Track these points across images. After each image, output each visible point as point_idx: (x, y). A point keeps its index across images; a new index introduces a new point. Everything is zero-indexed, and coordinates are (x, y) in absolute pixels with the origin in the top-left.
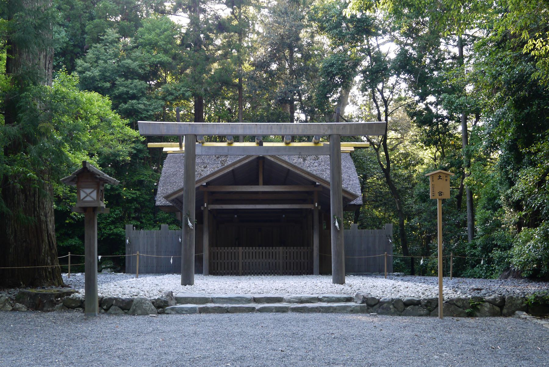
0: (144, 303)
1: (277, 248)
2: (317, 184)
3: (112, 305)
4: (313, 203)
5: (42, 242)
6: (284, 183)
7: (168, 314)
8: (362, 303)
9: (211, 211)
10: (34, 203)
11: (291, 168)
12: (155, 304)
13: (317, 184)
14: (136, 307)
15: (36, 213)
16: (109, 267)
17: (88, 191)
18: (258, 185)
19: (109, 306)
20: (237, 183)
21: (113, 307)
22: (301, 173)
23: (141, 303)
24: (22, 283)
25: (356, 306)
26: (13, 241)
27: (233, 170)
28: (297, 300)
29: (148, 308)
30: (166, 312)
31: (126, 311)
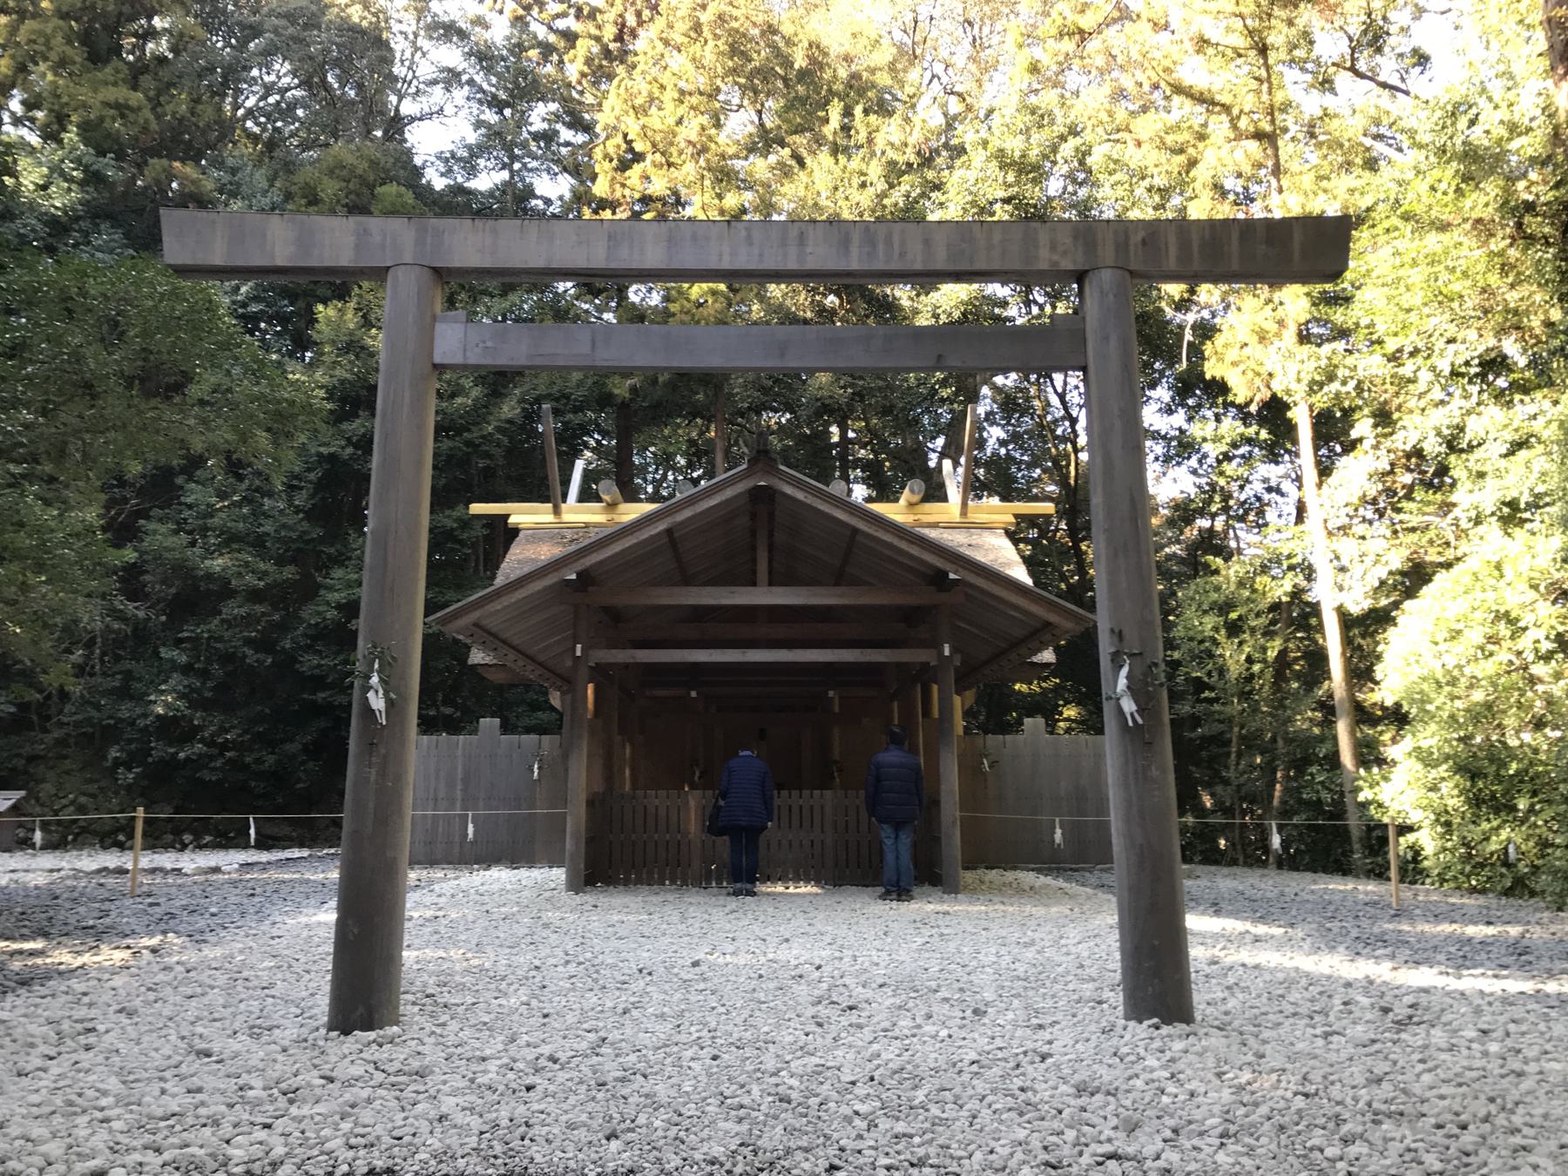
6: (839, 578)
13: (952, 576)
18: (754, 584)
20: (687, 580)
27: (669, 532)
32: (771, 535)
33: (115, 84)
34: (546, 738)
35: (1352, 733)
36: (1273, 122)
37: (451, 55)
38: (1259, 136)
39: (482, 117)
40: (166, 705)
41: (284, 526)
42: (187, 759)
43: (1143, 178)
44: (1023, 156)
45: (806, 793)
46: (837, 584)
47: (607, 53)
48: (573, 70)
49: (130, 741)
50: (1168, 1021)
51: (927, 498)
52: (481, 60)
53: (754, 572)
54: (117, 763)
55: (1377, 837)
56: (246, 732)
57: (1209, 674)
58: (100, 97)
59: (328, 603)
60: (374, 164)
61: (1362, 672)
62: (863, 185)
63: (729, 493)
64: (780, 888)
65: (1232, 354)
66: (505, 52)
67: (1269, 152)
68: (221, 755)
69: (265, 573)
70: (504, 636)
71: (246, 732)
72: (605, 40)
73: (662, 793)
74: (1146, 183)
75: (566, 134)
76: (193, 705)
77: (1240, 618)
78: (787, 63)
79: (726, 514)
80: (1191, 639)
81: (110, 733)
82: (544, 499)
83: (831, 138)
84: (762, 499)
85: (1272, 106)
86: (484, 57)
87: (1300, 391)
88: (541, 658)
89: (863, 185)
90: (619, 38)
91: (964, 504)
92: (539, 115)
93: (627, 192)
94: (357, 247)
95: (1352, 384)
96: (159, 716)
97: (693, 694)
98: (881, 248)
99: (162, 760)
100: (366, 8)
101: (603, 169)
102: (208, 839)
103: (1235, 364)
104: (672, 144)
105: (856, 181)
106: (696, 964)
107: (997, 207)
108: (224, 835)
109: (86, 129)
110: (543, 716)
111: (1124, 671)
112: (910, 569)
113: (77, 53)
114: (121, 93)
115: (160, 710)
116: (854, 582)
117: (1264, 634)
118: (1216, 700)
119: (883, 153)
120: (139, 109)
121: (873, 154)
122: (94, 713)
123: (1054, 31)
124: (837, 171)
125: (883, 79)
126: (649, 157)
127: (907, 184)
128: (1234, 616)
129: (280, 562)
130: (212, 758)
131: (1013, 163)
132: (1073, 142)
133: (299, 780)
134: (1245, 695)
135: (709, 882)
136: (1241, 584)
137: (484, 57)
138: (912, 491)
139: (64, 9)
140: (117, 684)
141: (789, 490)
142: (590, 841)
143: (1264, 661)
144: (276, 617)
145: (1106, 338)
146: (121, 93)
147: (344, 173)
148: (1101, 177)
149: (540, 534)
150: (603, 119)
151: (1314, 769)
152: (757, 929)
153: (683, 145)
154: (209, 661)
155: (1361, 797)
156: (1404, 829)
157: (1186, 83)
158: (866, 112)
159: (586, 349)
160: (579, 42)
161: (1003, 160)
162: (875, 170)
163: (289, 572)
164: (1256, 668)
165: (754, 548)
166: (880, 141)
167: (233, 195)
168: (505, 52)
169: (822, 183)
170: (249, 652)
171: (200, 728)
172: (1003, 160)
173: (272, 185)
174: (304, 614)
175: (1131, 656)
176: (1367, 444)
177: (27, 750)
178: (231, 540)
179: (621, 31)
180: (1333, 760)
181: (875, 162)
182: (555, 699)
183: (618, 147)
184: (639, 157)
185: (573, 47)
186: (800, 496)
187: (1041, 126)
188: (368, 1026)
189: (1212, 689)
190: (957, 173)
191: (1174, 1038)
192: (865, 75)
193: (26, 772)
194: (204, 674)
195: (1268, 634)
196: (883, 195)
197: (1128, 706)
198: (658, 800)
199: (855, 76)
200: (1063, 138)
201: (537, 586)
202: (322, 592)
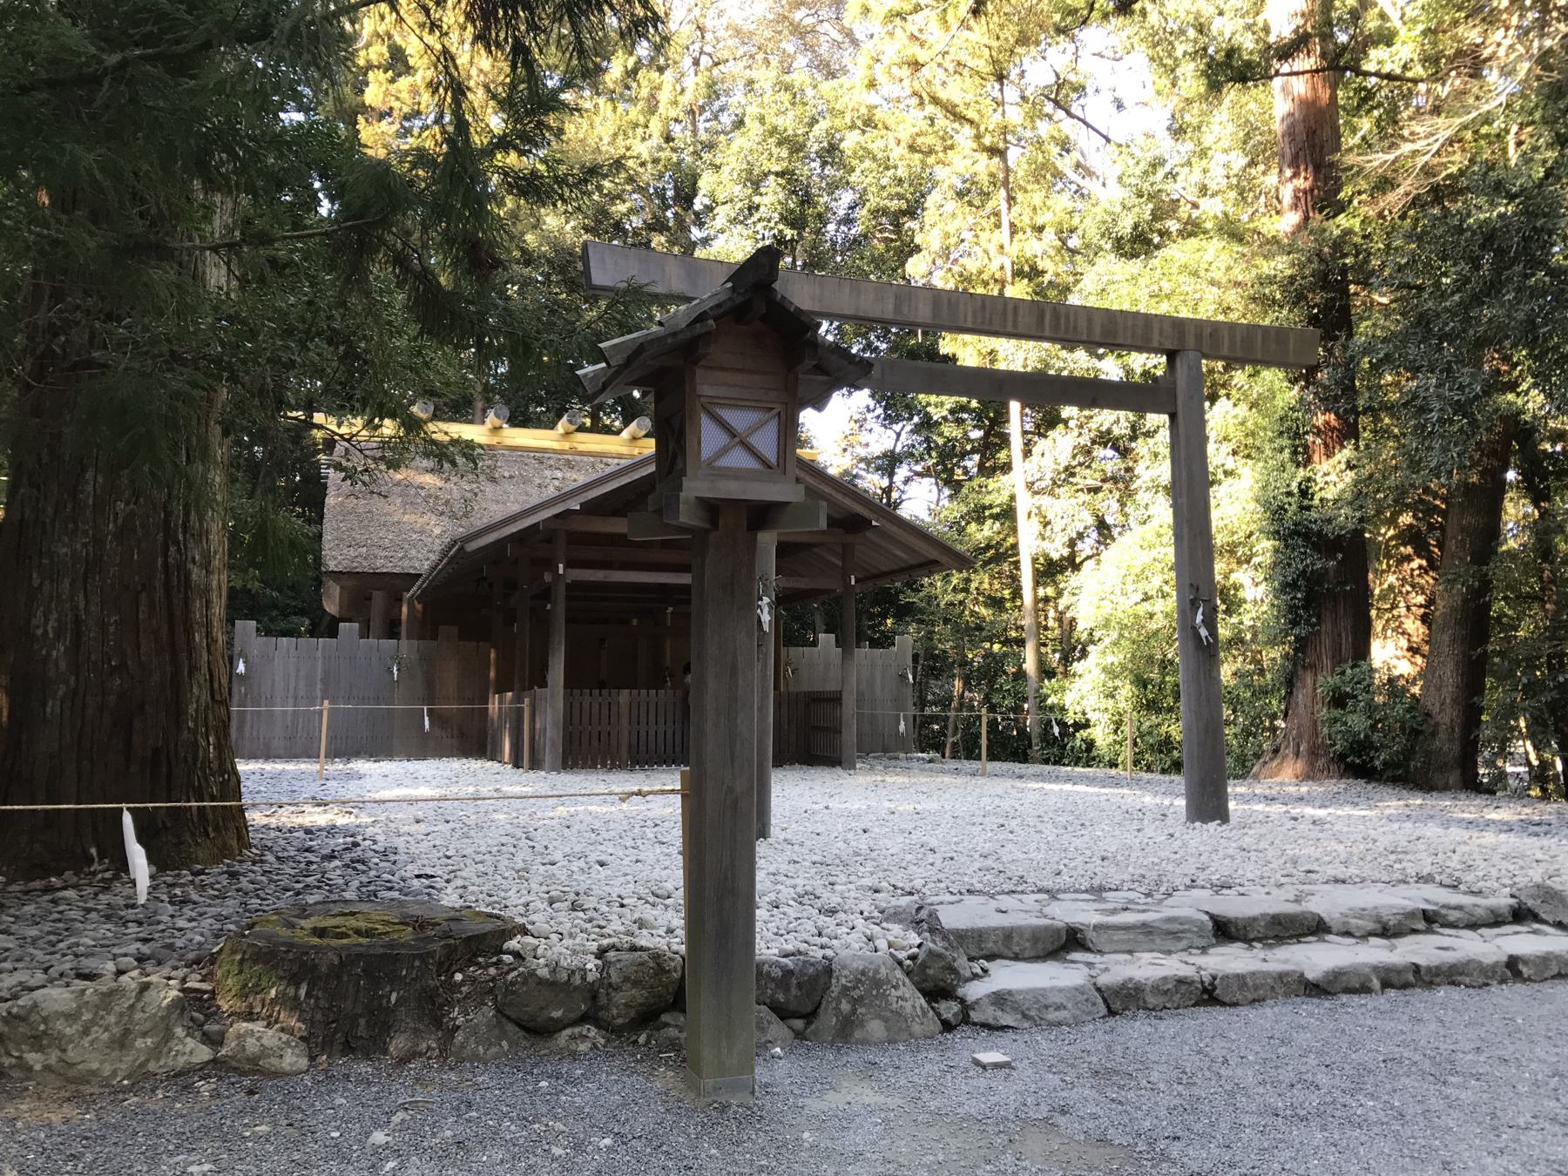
5: (191, 673)
9: (574, 586)
10: (168, 514)
14: (855, 1002)
15: (173, 549)
24: (93, 851)
26: (63, 665)
28: (1371, 926)
31: (799, 1024)
107: (772, 178)
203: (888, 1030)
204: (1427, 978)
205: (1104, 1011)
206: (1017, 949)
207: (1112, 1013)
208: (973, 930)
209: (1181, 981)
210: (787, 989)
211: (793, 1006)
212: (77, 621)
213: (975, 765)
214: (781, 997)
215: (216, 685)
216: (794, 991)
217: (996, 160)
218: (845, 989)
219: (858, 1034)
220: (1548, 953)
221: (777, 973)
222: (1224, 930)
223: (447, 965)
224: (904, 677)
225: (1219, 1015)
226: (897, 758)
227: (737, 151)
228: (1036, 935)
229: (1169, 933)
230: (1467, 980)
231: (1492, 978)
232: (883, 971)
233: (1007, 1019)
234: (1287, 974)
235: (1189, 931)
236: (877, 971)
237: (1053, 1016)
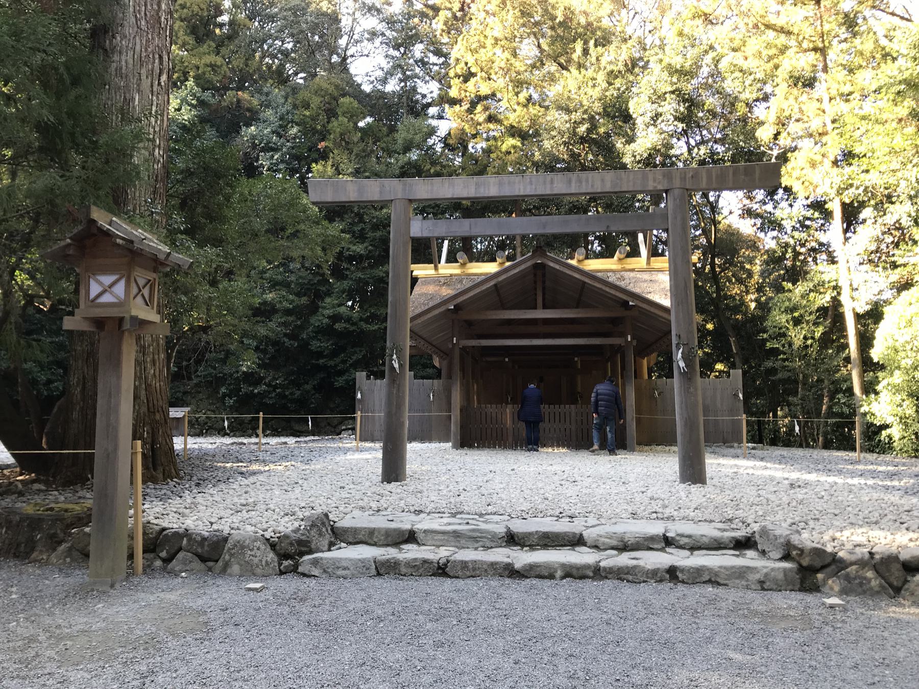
0: (248, 547)
1: (567, 406)
2: (631, 303)
3: (180, 549)
4: (623, 335)
6: (578, 304)
7: (304, 575)
8: (781, 559)
9: (464, 349)
11: (587, 280)
12: (278, 548)
13: (631, 303)
14: (232, 555)
16: (349, 429)
17: (107, 280)
18: (536, 308)
19: (173, 551)
20: (504, 306)
21: (181, 555)
22: (604, 288)
23: (243, 547)
25: (773, 569)
26: (79, 396)
27: (495, 285)
28: (614, 543)
29: (256, 560)
30: (300, 569)
31: (211, 564)
32: (544, 282)
33: (209, 54)
34: (436, 381)
35: (862, 377)
36: (823, 41)
37: (371, 22)
38: (815, 49)
39: (389, 53)
40: (248, 367)
41: (301, 277)
42: (259, 393)
43: (750, 74)
44: (682, 67)
45: (562, 406)
46: (577, 307)
47: (455, 17)
48: (438, 25)
49: (229, 385)
50: (694, 483)
51: (629, 255)
52: (388, 23)
53: (536, 304)
54: (224, 395)
55: (873, 432)
56: (285, 380)
57: (783, 346)
58: (203, 61)
59: (323, 315)
60: (337, 87)
61: (866, 341)
62: (594, 86)
63: (523, 267)
64: (550, 450)
65: (796, 174)
66: (400, 17)
67: (821, 59)
68: (274, 391)
69: (293, 301)
70: (420, 334)
71: (285, 380)
72: (454, 10)
73: (494, 406)
74: (752, 77)
75: (433, 59)
76: (259, 366)
77: (801, 316)
78: (553, 18)
79: (522, 275)
80: (775, 327)
81: (220, 381)
82: (430, 262)
83: (576, 60)
84: (540, 268)
85: (823, 33)
86: (391, 22)
87: (832, 193)
88: (434, 343)
89: (594, 86)
90: (462, 9)
91: (648, 259)
92: (418, 50)
93: (468, 94)
94: (381, 192)
95: (862, 189)
96: (244, 372)
97: (507, 360)
98: (584, 183)
99: (246, 393)
100: (330, 2)
101: (455, 82)
102: (268, 432)
103: (798, 179)
104: (491, 68)
105: (590, 84)
106: (513, 470)
107: (667, 96)
108: (276, 430)
109: (197, 78)
110: (430, 371)
111: (681, 351)
112: (610, 298)
113: (191, 40)
114: (212, 59)
115: (245, 369)
116: (587, 306)
117: (814, 324)
118: (787, 359)
119: (605, 68)
120: (222, 65)
121: (600, 68)
122: (212, 371)
123: (690, 16)
124: (580, 77)
125: (606, 23)
126: (479, 75)
127: (618, 83)
128: (796, 314)
129: (298, 295)
130: (269, 392)
131: (676, 71)
132: (712, 54)
133: (312, 403)
134: (803, 357)
135: (516, 447)
136: (803, 297)
137: (391, 22)
138: (620, 252)
139: (183, 17)
140: (222, 356)
141: (552, 264)
142: (461, 427)
143: (813, 338)
144: (299, 323)
145: (676, 218)
146: (212, 59)
147: (323, 93)
148: (726, 75)
149: (428, 280)
150: (455, 54)
151: (840, 396)
152: (538, 462)
153: (497, 70)
154: (267, 345)
155: (862, 410)
156: (886, 426)
157: (773, 22)
158: (596, 46)
159: (468, 229)
160: (441, 13)
161: (672, 70)
162: (601, 77)
163: (304, 300)
164: (809, 342)
165: (536, 289)
166: (604, 61)
167: (267, 106)
168: (400, 17)
169: (572, 85)
170: (286, 340)
171: (263, 378)
172: (672, 70)
173: (286, 100)
174: (312, 321)
175: (683, 345)
176: (869, 222)
177: (182, 389)
178: (275, 285)
179: (463, 5)
180: (850, 391)
181: (601, 72)
182: (436, 362)
183: (462, 69)
184: (473, 75)
185: (437, 15)
186: (557, 267)
187: (693, 46)
188: (397, 481)
189: (785, 354)
190: (646, 78)
191: (695, 489)
192: (595, 23)
193: (182, 400)
194: (264, 352)
195: (816, 324)
196: (606, 90)
197: (682, 364)
198: (492, 409)
199: (589, 24)
200: (706, 52)
201: (436, 312)
202: (320, 310)
203: (241, 570)
204: (603, 574)
205: (374, 572)
206: (376, 540)
207: (379, 574)
208: (352, 528)
209: (425, 561)
210: (203, 547)
211: (206, 555)
212: (84, 378)
213: (852, 455)
214: (199, 550)
215: (151, 405)
216: (206, 548)
217: (818, 55)
218: (229, 549)
219: (229, 571)
220: (704, 566)
221: (199, 538)
222: (512, 539)
223: (72, 525)
224: (736, 395)
225: (448, 584)
226: (732, 447)
227: (655, 78)
228: (388, 533)
229: (471, 537)
230: (630, 578)
231: (652, 578)
232: (247, 542)
233: (315, 572)
234: (496, 563)
235: (485, 537)
236: (244, 542)
237: (340, 572)
